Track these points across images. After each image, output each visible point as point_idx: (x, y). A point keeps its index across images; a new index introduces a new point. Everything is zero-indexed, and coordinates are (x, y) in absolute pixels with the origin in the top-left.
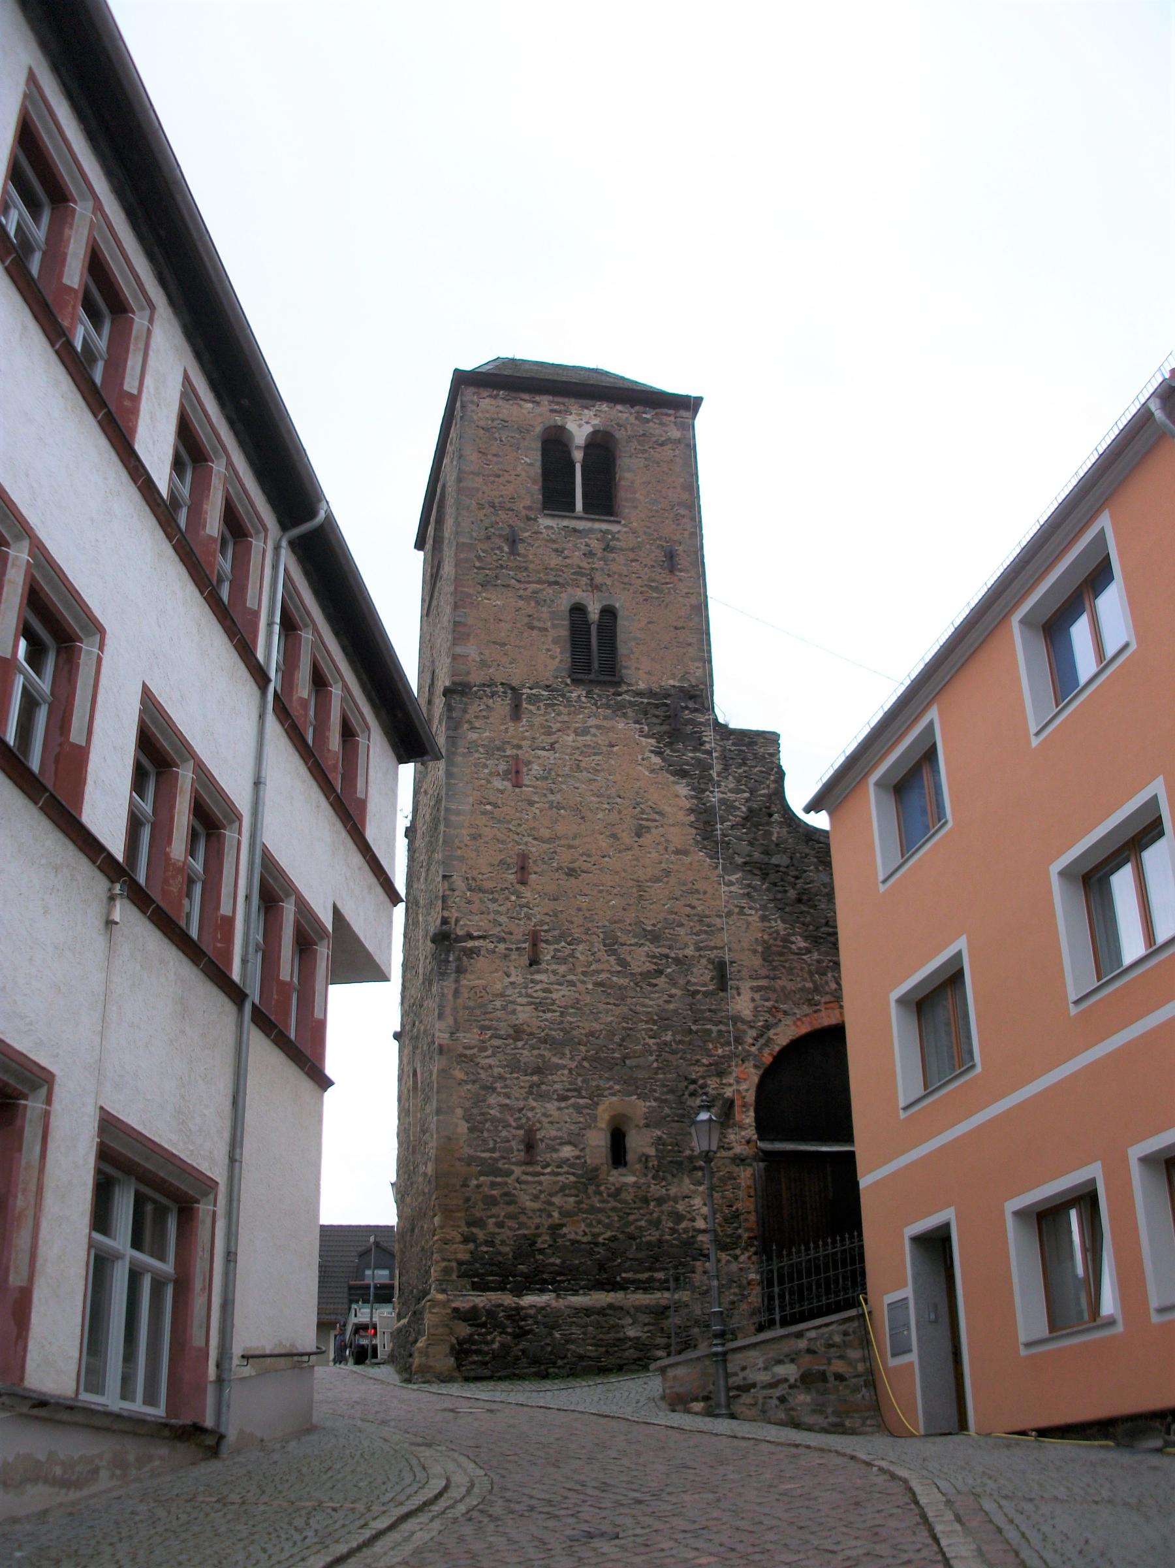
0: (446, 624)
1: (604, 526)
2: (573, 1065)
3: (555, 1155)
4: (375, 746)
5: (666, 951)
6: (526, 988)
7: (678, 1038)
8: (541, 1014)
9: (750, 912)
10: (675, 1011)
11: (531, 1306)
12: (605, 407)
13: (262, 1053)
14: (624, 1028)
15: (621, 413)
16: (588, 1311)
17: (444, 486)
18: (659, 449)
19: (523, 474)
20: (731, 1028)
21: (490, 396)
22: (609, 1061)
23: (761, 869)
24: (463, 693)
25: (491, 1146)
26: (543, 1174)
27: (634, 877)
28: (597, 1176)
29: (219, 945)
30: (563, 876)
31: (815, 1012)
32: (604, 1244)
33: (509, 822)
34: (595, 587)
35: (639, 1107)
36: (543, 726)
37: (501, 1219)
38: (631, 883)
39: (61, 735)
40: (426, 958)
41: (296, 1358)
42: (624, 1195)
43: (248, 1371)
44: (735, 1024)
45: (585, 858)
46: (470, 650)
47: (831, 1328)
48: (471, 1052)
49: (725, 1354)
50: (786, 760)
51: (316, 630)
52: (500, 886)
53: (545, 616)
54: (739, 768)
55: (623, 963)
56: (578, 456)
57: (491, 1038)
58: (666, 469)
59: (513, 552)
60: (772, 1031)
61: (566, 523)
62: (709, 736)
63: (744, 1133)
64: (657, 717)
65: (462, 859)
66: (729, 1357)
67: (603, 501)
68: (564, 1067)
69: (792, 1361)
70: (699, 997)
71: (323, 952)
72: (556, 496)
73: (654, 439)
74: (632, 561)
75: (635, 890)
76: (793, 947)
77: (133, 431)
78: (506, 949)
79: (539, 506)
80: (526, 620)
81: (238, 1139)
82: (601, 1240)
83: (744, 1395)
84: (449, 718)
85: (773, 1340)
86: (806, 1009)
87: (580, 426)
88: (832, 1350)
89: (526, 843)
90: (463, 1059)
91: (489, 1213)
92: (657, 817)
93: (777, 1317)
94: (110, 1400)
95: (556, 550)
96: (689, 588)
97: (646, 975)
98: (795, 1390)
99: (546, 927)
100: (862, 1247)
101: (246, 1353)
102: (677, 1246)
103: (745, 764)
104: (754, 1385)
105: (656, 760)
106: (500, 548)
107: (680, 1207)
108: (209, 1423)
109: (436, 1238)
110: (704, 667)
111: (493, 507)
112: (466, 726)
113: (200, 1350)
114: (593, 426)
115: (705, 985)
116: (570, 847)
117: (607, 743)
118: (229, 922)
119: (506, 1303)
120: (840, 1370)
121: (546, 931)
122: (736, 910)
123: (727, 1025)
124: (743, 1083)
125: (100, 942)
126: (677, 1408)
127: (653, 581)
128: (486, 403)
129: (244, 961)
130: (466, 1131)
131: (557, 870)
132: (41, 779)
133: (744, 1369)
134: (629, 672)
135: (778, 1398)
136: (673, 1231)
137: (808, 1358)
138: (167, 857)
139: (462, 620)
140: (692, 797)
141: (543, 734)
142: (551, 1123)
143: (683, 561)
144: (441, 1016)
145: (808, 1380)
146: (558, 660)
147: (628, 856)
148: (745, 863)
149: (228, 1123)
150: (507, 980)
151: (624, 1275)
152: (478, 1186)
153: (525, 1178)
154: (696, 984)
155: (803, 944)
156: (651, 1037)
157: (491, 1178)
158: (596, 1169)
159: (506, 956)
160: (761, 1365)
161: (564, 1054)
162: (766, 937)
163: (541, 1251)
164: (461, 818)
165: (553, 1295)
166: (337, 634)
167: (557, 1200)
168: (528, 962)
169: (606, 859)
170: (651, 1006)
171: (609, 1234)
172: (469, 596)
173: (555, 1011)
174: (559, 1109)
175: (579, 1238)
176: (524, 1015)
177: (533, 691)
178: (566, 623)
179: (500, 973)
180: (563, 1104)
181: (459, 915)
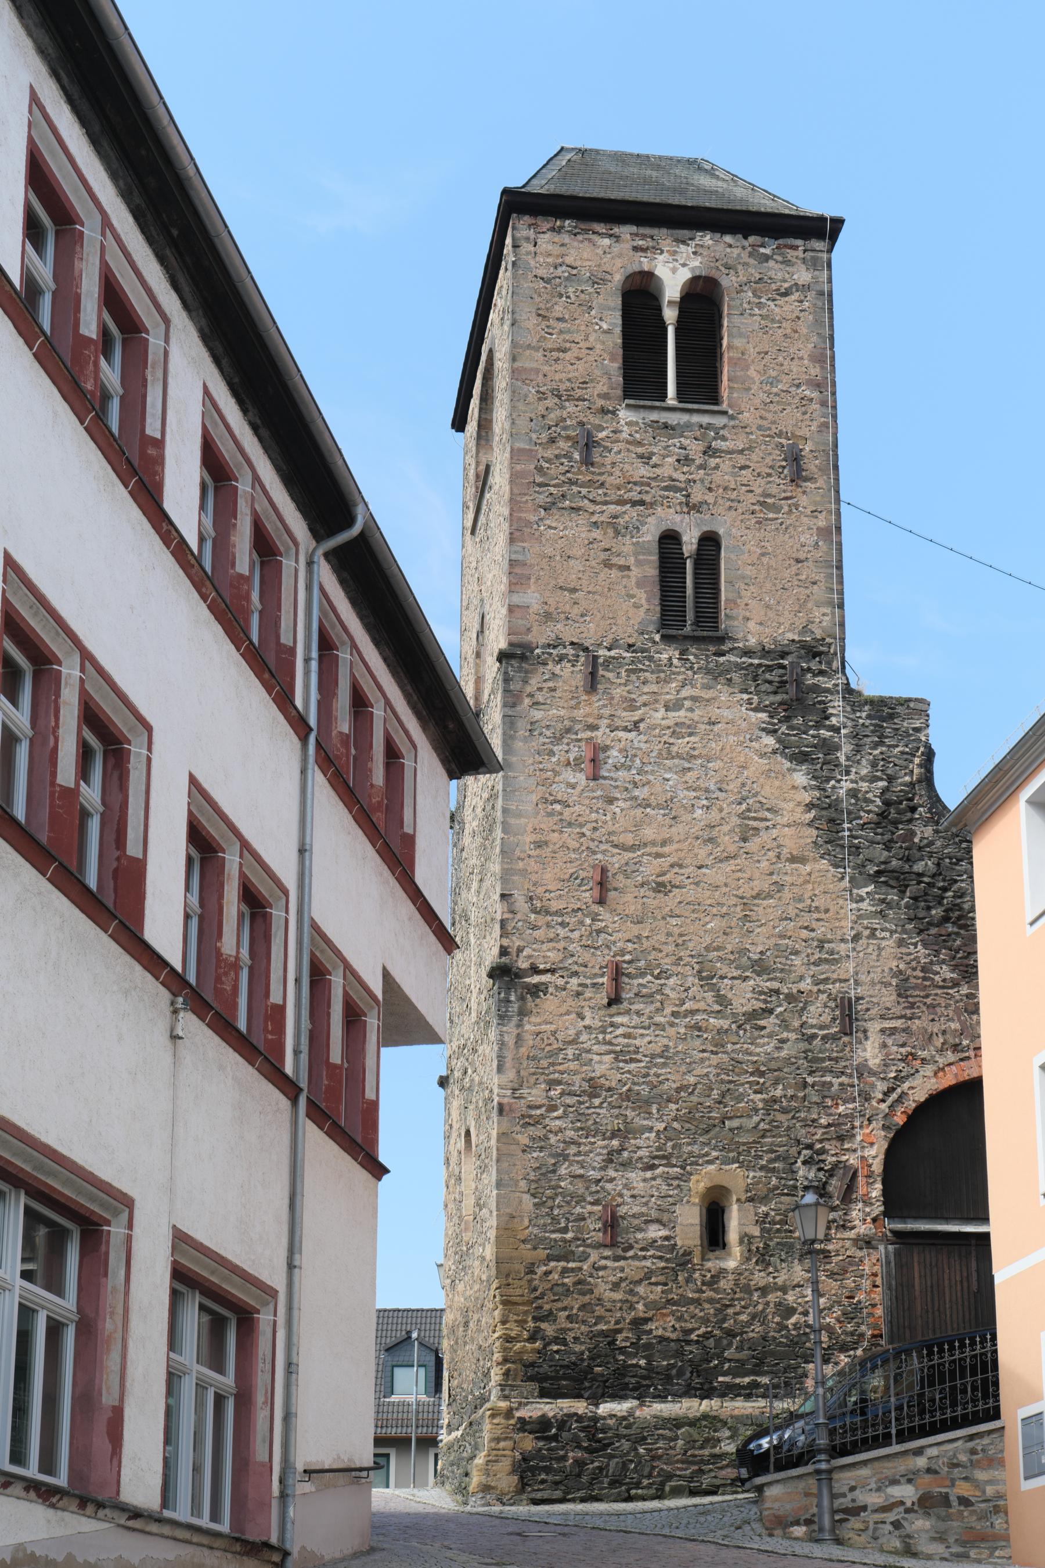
0: (499, 558)
1: (705, 419)
2: (661, 1126)
3: (639, 1236)
4: (425, 764)
5: (775, 985)
6: (604, 1032)
7: (790, 1092)
8: (621, 1065)
9: (883, 934)
10: (787, 1061)
11: (612, 1416)
12: (707, 239)
13: (317, 1143)
14: (722, 1082)
15: (728, 247)
16: (677, 1423)
17: (491, 351)
18: (782, 301)
19: (598, 346)
20: (856, 1081)
21: (553, 229)
22: (705, 1123)
23: (897, 879)
24: (523, 658)
25: (563, 1225)
26: (625, 1258)
27: (740, 893)
28: (689, 1261)
29: (270, 1037)
30: (652, 894)
31: (962, 1060)
32: (697, 1342)
33: (581, 826)
34: (692, 507)
35: (738, 1178)
36: (625, 699)
37: (575, 1311)
38: (733, 901)
39: (118, 849)
40: (480, 992)
41: (353, 1473)
42: (723, 1284)
43: (307, 1487)
44: (860, 1076)
45: (676, 870)
46: (531, 598)
47: (956, 1445)
48: (538, 1112)
49: (830, 1472)
50: (938, 735)
51: (354, 646)
52: (572, 906)
53: (628, 548)
54: (875, 748)
55: (721, 999)
56: (670, 315)
57: (562, 1094)
58: (788, 331)
59: (587, 461)
60: (906, 1085)
61: (654, 416)
62: (837, 706)
63: (865, 1213)
64: (770, 682)
65: (524, 872)
66: (835, 1476)
67: (702, 384)
68: (650, 1129)
69: (910, 1481)
70: (817, 1042)
71: (373, 1022)
72: (640, 380)
73: (774, 287)
74: (742, 468)
75: (739, 909)
76: (937, 978)
77: (159, 486)
78: (580, 985)
79: (619, 392)
80: (603, 556)
81: (297, 1244)
82: (693, 1337)
83: (852, 1519)
84: (506, 691)
85: (887, 1457)
86: (951, 1056)
87: (674, 271)
88: (956, 1470)
89: (604, 852)
90: (528, 1121)
91: (559, 1305)
92: (769, 815)
93: (894, 1431)
94: (182, 1513)
95: (641, 456)
96: (816, 503)
97: (753, 1015)
98: (912, 1515)
99: (627, 957)
100: (996, 1351)
101: (306, 1468)
102: (787, 1345)
103: (881, 743)
104: (864, 1508)
105: (770, 741)
106: (568, 456)
107: (790, 1298)
108: (274, 1540)
109: (496, 1335)
110: (833, 614)
111: (559, 397)
112: (527, 701)
113: (263, 1464)
114: (692, 270)
115: (821, 1028)
116: (658, 855)
117: (706, 720)
118: (281, 1009)
119: (580, 1412)
120: (966, 1494)
121: (630, 962)
122: (867, 932)
123: (851, 1076)
124: (869, 1149)
125: (167, 1058)
126: (776, 1532)
127: (769, 496)
128: (546, 242)
129: (297, 1052)
130: (531, 1207)
131: (642, 885)
132: (99, 897)
133: (852, 1489)
134: (736, 623)
135: (892, 1523)
136: (782, 1327)
137: (928, 1478)
138: (218, 953)
139: (520, 557)
140: (812, 788)
141: (624, 709)
142: (633, 1196)
143: (811, 465)
144: (500, 1069)
145: (926, 1503)
146: (643, 610)
147: (729, 867)
148: (879, 873)
149: (285, 1228)
150: (582, 1024)
151: (720, 1379)
152: (547, 1273)
153: (603, 1262)
154: (812, 1027)
155: (950, 975)
156: (756, 1092)
157: (563, 1264)
158: (688, 1253)
159: (578, 994)
160: (873, 1486)
161: (650, 1113)
162: (902, 966)
163: (622, 1350)
164: (523, 821)
165: (636, 1403)
166: (377, 643)
167: (641, 1290)
168: (605, 1001)
169: (704, 870)
170: (758, 1055)
171: (703, 1330)
172: (529, 524)
173: (641, 1061)
174: (645, 1180)
175: (667, 1334)
176: (602, 1066)
177: (613, 653)
178: (655, 558)
179: (574, 1016)
180: (649, 1174)
181: (522, 944)
